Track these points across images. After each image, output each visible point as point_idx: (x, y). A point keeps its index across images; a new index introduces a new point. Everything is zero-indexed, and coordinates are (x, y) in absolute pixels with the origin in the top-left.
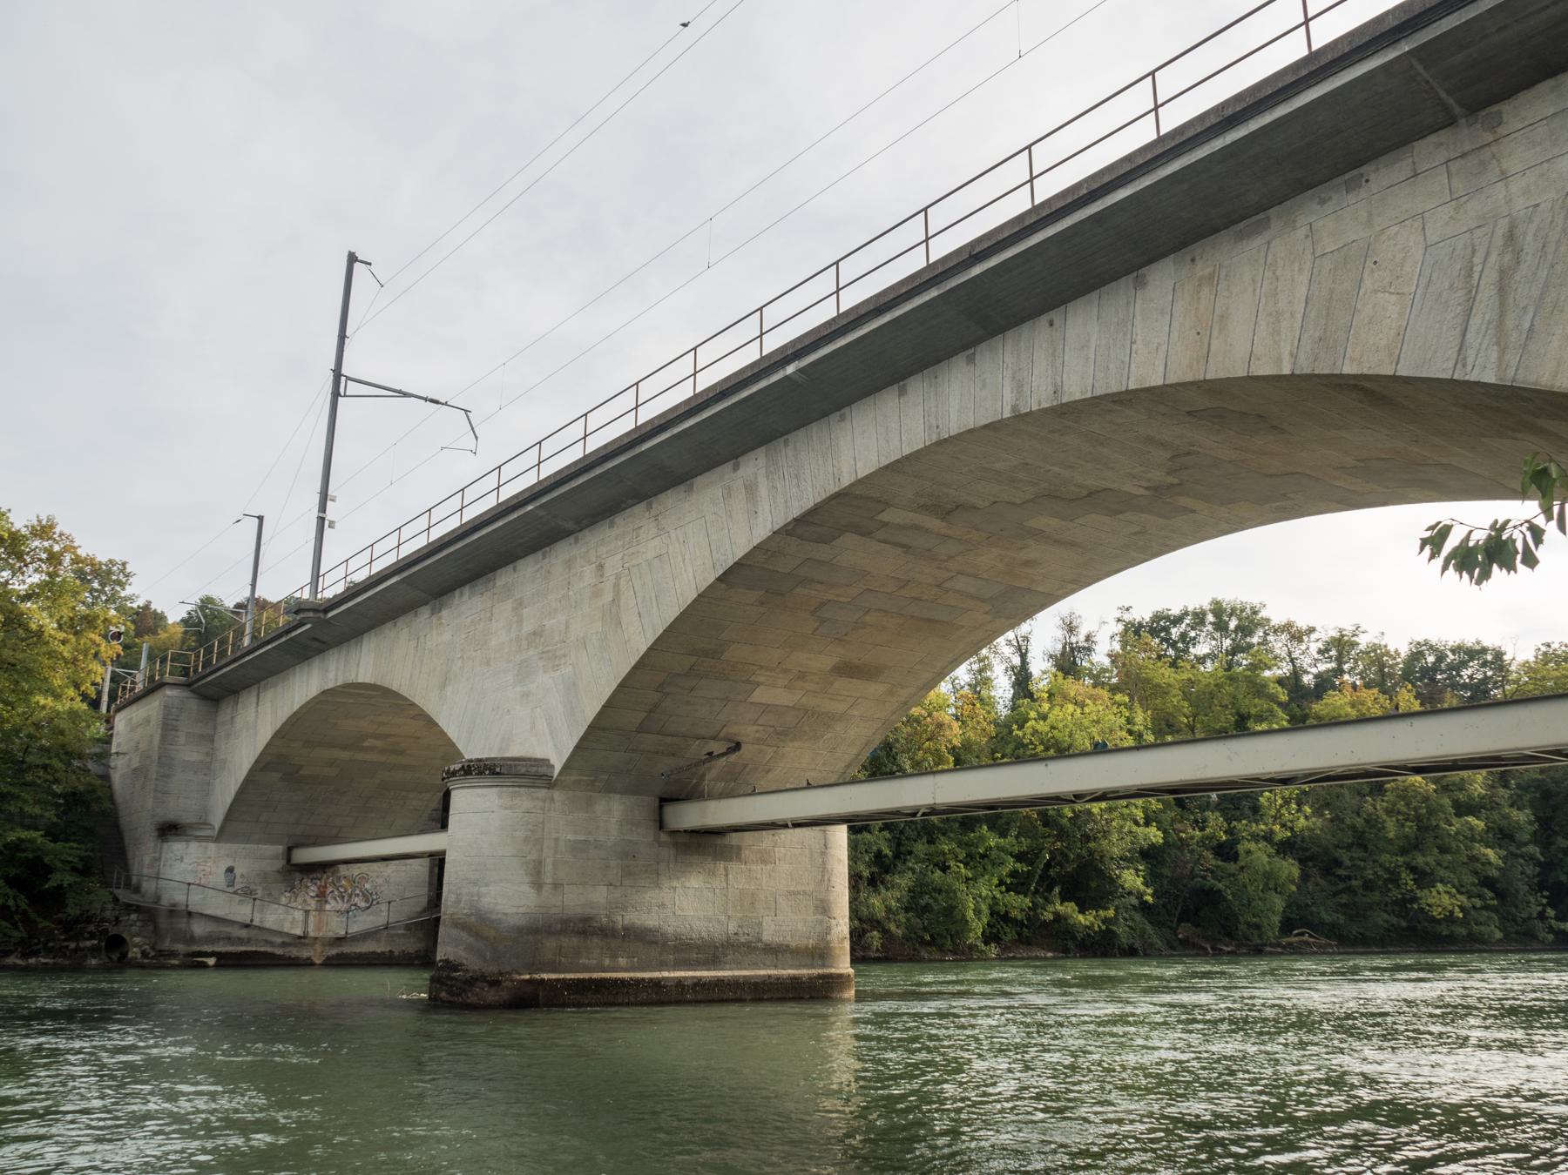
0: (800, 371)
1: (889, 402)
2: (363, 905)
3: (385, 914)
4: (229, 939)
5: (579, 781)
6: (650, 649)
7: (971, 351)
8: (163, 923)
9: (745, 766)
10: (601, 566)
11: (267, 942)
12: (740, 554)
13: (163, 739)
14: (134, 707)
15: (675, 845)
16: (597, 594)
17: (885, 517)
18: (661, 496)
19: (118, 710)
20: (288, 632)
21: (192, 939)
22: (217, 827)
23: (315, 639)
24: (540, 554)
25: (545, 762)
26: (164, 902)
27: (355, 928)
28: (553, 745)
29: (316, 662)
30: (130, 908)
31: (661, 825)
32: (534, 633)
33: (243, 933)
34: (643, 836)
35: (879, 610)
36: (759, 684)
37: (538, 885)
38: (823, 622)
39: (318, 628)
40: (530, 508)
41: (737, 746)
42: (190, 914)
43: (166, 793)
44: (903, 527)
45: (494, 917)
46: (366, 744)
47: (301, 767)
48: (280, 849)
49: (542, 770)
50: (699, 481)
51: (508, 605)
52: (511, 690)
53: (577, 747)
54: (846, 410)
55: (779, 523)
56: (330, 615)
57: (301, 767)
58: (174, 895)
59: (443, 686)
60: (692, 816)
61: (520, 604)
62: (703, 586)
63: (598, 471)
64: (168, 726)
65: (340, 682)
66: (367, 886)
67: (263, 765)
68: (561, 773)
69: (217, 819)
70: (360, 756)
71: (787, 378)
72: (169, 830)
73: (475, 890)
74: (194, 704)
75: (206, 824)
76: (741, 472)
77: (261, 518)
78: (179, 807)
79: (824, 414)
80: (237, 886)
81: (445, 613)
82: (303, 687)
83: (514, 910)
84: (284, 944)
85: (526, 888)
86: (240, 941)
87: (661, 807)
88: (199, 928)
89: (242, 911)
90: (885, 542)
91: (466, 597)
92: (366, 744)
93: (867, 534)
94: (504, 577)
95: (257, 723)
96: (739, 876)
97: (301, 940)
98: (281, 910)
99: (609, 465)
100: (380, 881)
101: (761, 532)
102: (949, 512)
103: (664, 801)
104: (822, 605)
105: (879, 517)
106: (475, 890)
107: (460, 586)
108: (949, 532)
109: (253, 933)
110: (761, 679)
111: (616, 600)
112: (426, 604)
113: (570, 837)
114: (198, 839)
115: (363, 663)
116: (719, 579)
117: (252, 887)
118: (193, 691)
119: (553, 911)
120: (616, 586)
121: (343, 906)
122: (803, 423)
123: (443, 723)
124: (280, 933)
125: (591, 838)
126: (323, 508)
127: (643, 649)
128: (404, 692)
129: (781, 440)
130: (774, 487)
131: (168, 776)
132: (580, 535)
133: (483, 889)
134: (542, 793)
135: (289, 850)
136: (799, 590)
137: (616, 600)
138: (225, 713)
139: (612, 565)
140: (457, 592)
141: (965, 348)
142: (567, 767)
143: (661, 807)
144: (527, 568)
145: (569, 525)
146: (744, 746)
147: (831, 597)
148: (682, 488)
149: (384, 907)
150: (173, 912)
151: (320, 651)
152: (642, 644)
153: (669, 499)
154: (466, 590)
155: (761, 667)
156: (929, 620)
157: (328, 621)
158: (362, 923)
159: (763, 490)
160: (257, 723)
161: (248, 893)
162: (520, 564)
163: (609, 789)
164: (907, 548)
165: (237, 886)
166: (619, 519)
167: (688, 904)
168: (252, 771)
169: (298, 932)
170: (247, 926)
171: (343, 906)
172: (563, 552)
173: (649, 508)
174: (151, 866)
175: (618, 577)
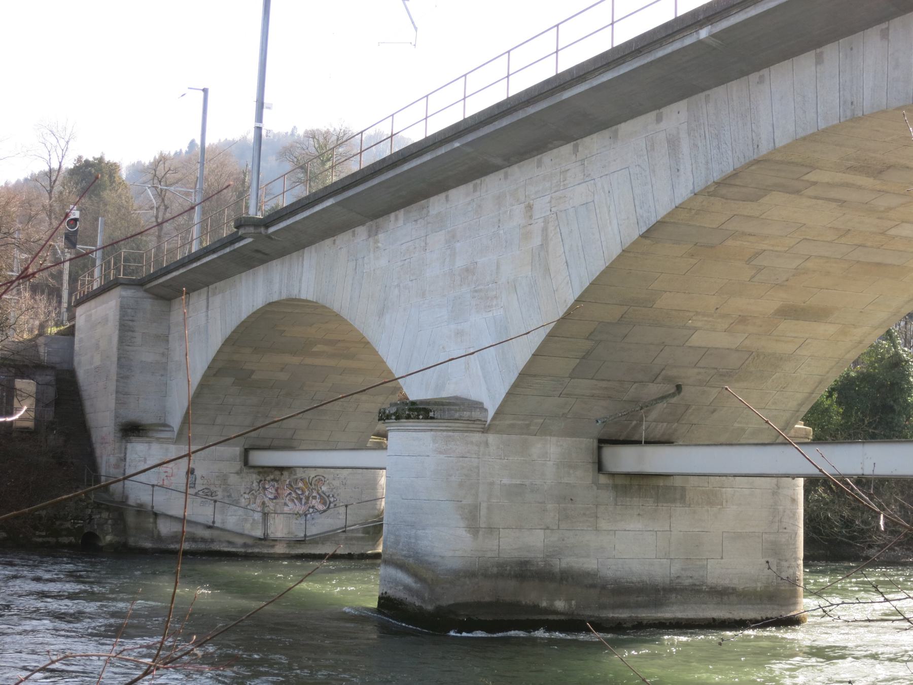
0: (714, 36)
1: (804, 67)
2: (321, 507)
3: (343, 517)
4: (194, 539)
5: (512, 426)
6: (577, 301)
7: (884, 26)
8: (131, 520)
9: (688, 407)
10: (530, 207)
11: (230, 543)
12: (662, 213)
13: (121, 340)
14: (92, 303)
15: (615, 487)
16: (526, 236)
17: (812, 177)
18: (587, 140)
19: (79, 303)
20: (232, 242)
21: (159, 538)
22: (176, 429)
23: (257, 251)
24: (470, 185)
25: (478, 406)
26: (131, 502)
27: (313, 531)
28: (485, 383)
29: (261, 270)
30: (98, 506)
31: (600, 467)
32: (467, 270)
33: (207, 534)
34: (583, 476)
35: (821, 257)
36: (696, 329)
37: (474, 530)
38: (760, 269)
39: (258, 240)
40: (457, 144)
41: (679, 388)
42: (156, 515)
43: (127, 394)
44: (830, 185)
45: (431, 559)
46: (315, 349)
47: (253, 372)
48: (235, 450)
49: (476, 414)
50: (625, 128)
51: (438, 239)
52: (451, 312)
53: (509, 394)
54: (765, 72)
55: (700, 185)
56: (272, 230)
57: (253, 372)
58: (138, 493)
59: (381, 314)
60: (626, 459)
61: (452, 237)
62: (628, 242)
63: (521, 115)
64: (125, 328)
65: (284, 297)
66: (324, 488)
67: (215, 371)
68: (494, 418)
69: (175, 421)
70: (309, 361)
71: (700, 42)
72: (132, 430)
73: (413, 532)
74: (148, 304)
75: (165, 425)
76: (663, 125)
77: (205, 91)
78: (141, 410)
79: (743, 73)
80: (199, 487)
81: (381, 236)
82: (252, 293)
83: (450, 554)
84: (245, 545)
85: (463, 533)
86: (203, 540)
87: (599, 449)
88: (165, 528)
89: (201, 512)
90: (816, 198)
91: (401, 222)
92: (315, 349)
93: (798, 192)
94: (437, 205)
95: (206, 326)
96: (681, 522)
97: (265, 539)
98: (241, 512)
99: (531, 110)
100: (336, 483)
101: (683, 193)
102: (881, 172)
103: (603, 442)
104: (757, 254)
105: (806, 177)
106: (413, 532)
107: (394, 210)
108: (885, 188)
109: (216, 533)
110: (699, 324)
111: (544, 246)
112: (362, 223)
113: (506, 481)
114: (158, 439)
115: (304, 277)
116: (644, 236)
117: (213, 488)
118: (146, 291)
119: (489, 555)
120: (545, 230)
121: (300, 508)
122: (723, 79)
123: (382, 350)
124: (241, 535)
125: (527, 482)
126: (259, 117)
127: (571, 300)
128: (344, 314)
129: (702, 95)
130: (695, 145)
131: (127, 377)
132: (509, 170)
133: (420, 532)
134: (477, 437)
135: (246, 451)
136: (729, 243)
137: (544, 246)
138: (178, 310)
139: (541, 207)
140: (393, 215)
141: (879, 21)
142: (499, 413)
143: (599, 449)
144: (459, 196)
145: (499, 161)
146: (685, 389)
147: (765, 247)
148: (606, 133)
149: (342, 510)
150: (141, 510)
151: (263, 262)
152: (570, 295)
153: (594, 143)
154: (401, 213)
155: (697, 313)
156: (878, 264)
157: (269, 237)
158: (321, 524)
159: (685, 147)
160: (206, 326)
161: (209, 494)
162: (454, 193)
163: (544, 431)
164: (842, 203)
165: (199, 487)
166: (547, 158)
167: (628, 546)
168: (205, 377)
169: (259, 533)
170: (209, 527)
171: (300, 508)
172: (493, 184)
173: (576, 150)
174: (117, 466)
175: (546, 221)
